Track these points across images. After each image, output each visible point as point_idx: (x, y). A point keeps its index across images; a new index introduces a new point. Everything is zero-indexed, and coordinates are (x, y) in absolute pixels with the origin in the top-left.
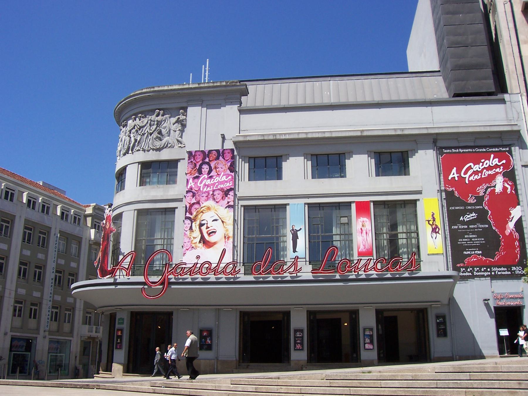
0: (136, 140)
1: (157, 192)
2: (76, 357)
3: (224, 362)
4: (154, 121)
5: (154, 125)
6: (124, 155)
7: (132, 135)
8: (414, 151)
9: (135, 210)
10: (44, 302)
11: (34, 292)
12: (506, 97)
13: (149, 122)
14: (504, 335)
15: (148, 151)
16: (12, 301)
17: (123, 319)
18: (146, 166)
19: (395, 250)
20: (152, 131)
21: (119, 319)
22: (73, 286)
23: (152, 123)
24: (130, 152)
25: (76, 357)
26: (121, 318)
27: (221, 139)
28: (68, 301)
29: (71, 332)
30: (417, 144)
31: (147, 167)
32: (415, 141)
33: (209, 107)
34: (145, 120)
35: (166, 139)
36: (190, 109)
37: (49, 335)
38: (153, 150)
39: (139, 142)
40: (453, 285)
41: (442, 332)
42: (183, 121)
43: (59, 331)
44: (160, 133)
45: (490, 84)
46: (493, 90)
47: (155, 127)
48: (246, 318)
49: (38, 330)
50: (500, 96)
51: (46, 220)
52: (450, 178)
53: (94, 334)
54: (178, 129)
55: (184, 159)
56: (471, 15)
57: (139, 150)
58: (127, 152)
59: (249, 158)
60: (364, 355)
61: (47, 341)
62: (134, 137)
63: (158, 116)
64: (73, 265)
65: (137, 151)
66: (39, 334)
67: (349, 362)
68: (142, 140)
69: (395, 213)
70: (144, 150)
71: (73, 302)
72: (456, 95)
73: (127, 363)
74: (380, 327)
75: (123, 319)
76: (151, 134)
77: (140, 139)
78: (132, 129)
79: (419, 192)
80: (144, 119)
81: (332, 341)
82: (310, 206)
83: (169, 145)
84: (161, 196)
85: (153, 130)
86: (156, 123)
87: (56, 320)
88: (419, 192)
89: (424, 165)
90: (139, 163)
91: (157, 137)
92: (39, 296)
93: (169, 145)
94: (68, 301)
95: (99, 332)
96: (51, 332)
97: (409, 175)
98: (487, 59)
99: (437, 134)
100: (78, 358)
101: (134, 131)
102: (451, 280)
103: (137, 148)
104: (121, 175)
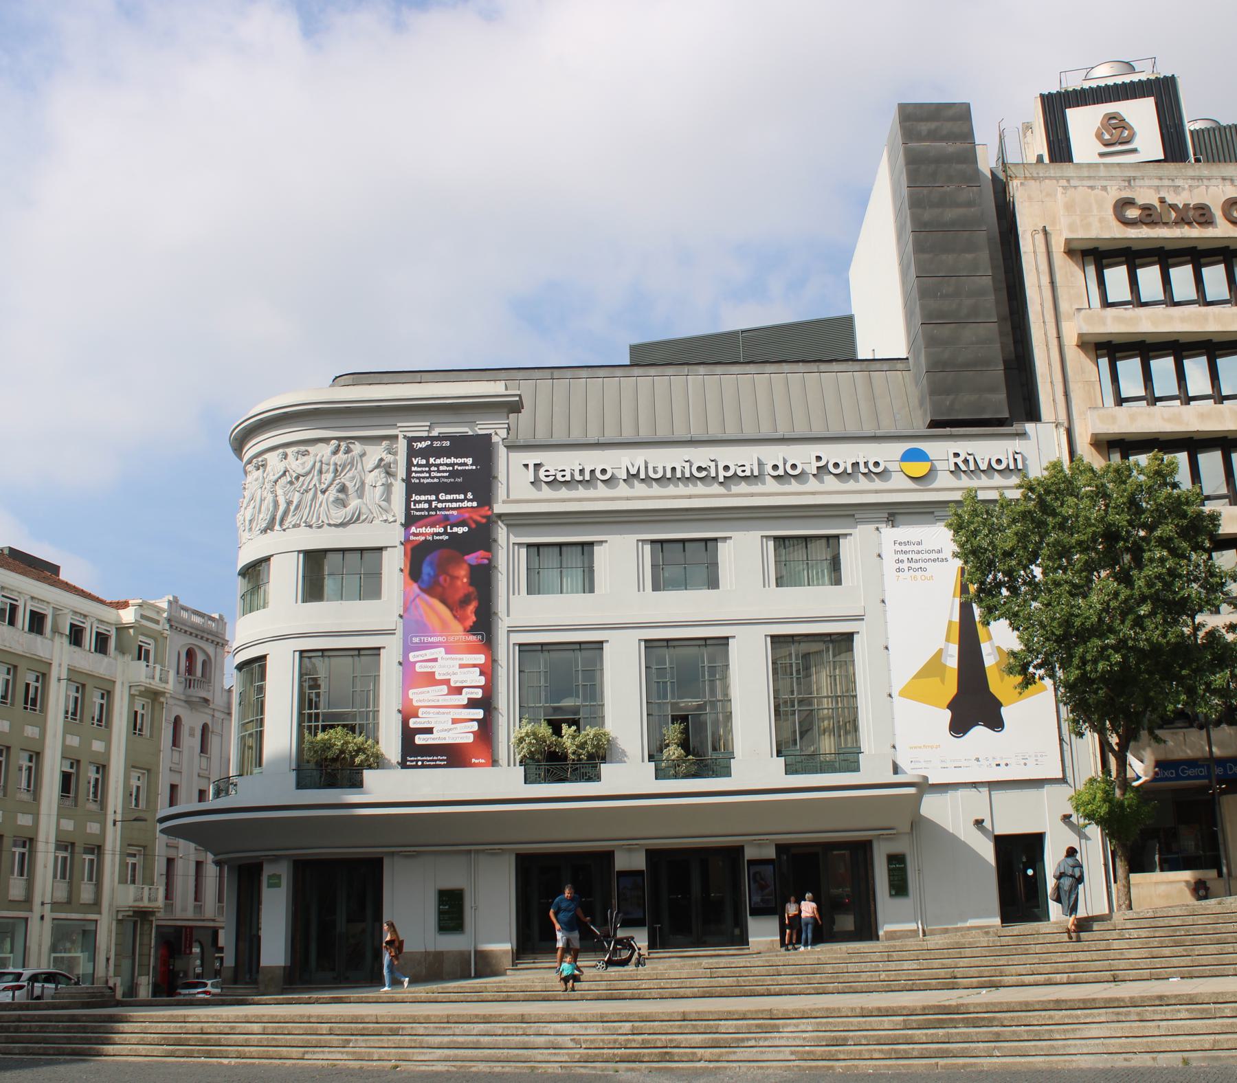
0: (289, 503)
1: (340, 617)
2: (108, 960)
4: (328, 464)
5: (328, 471)
6: (265, 531)
7: (280, 492)
10: (41, 837)
11: (20, 815)
12: (1030, 427)
13: (318, 465)
14: (1158, 876)
16: (52, 847)
17: (279, 877)
18: (314, 561)
20: (324, 486)
21: (270, 877)
23: (325, 468)
24: (277, 527)
25: (108, 960)
26: (274, 875)
28: (88, 831)
29: (96, 905)
31: (314, 561)
34: (309, 461)
35: (354, 503)
37: (52, 911)
38: (329, 525)
39: (297, 507)
40: (918, 800)
41: (899, 887)
42: (389, 465)
43: (70, 902)
44: (343, 489)
45: (998, 402)
46: (1006, 415)
47: (330, 476)
49: (28, 901)
50: (1016, 427)
51: (40, 646)
54: (379, 483)
56: (969, 256)
57: (299, 525)
58: (270, 527)
60: (69, 737)
61: (48, 924)
63: (335, 452)
65: (294, 526)
66: (31, 910)
68: (303, 504)
71: (98, 832)
72: (934, 424)
76: (323, 492)
77: (300, 502)
79: (859, 618)
80: (305, 458)
82: (649, 644)
85: (327, 483)
86: (332, 468)
87: (63, 877)
88: (859, 618)
91: (337, 500)
92: (98, 832)
93: (363, 517)
94: (88, 831)
95: (156, 900)
96: (56, 906)
100: (112, 962)
101: (283, 480)
102: (912, 790)
103: (290, 520)
104: (255, 572)
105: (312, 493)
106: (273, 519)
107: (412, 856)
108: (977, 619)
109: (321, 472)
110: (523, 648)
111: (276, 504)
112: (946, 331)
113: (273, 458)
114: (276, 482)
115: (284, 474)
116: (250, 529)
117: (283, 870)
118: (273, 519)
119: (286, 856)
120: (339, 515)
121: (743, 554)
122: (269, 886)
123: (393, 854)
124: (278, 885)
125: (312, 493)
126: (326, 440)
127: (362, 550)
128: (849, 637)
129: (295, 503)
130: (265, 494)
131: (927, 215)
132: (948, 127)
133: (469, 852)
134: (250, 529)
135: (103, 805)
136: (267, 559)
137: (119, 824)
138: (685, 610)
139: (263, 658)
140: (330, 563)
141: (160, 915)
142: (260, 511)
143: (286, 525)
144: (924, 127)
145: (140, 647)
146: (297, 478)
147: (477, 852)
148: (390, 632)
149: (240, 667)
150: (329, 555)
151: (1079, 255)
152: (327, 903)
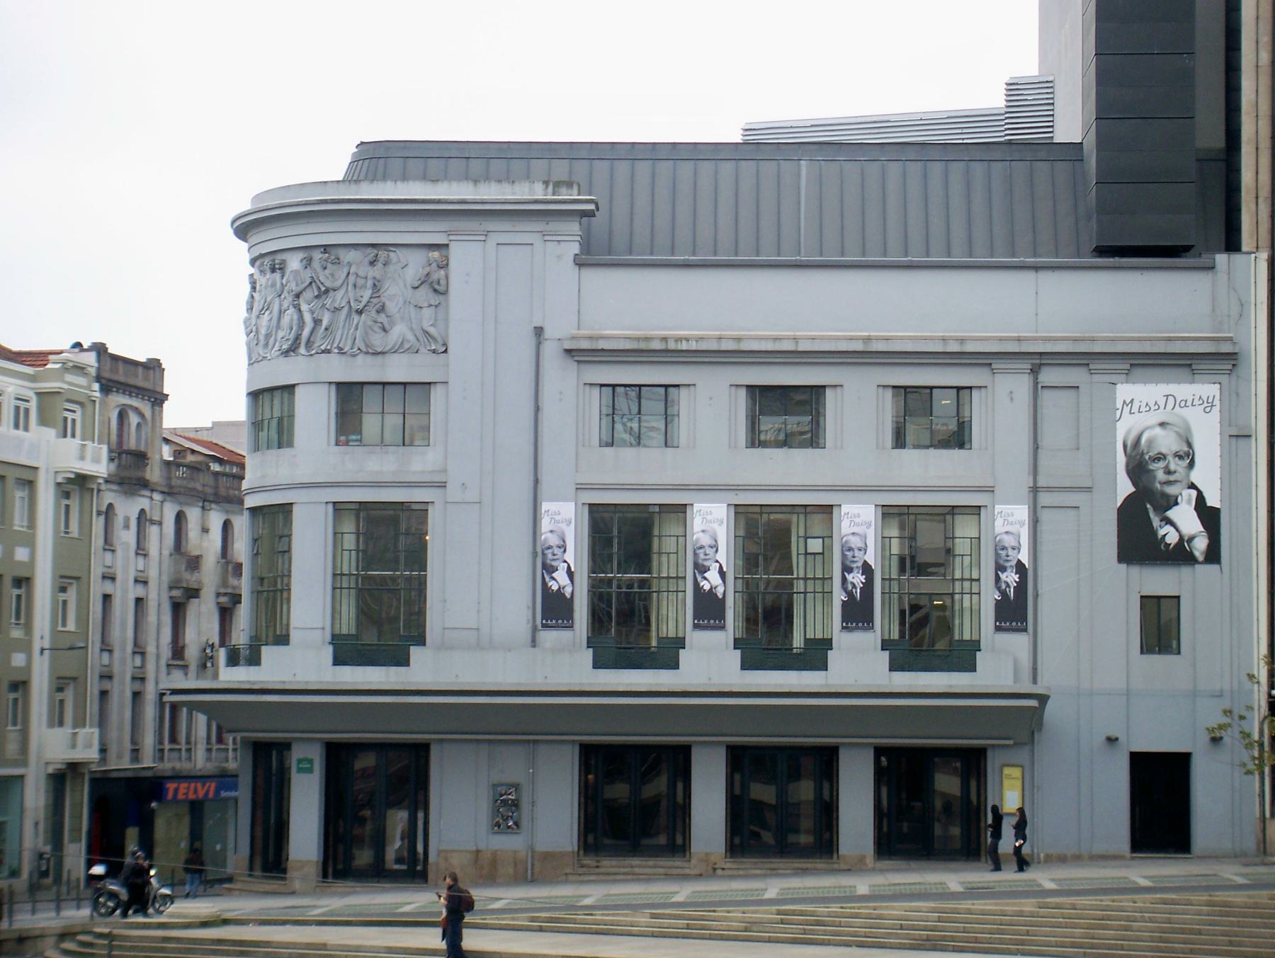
0: (317, 322)
3: (547, 856)
6: (286, 353)
7: (304, 307)
12: (1221, 259)
17: (311, 761)
20: (361, 307)
24: (302, 350)
27: (531, 340)
31: (349, 397)
48: (679, 841)
50: (1204, 260)
53: (79, 755)
57: (329, 352)
58: (292, 350)
59: (602, 385)
60: (1244, 248)
62: (313, 313)
64: (21, 554)
65: (323, 352)
67: (1098, 84)
70: (341, 352)
73: (321, 859)
74: (884, 791)
75: (311, 761)
76: (360, 312)
81: (781, 797)
83: (407, 346)
86: (370, 283)
88: (990, 490)
106: (298, 337)
110: (595, 508)
113: (294, 263)
114: (298, 296)
116: (266, 345)
117: (316, 755)
118: (298, 337)
121: (858, 409)
122: (300, 770)
123: (442, 741)
124: (310, 771)
127: (405, 384)
129: (325, 323)
134: (266, 345)
135: (28, 627)
137: (46, 652)
138: (784, 474)
140: (370, 400)
141: (94, 768)
142: (278, 327)
145: (66, 419)
146: (327, 291)
150: (366, 388)
152: (374, 794)
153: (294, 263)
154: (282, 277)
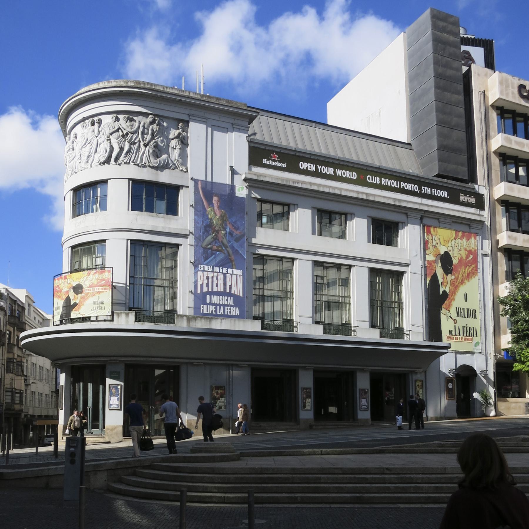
0: (122, 149)
6: (104, 163)
8: (405, 224)
9: (127, 240)
13: (141, 129)
15: (144, 166)
19: (384, 308)
22: (22, 335)
30: (408, 217)
32: (438, 219)
33: (216, 127)
36: (192, 125)
38: (149, 166)
46: (467, 178)
47: (149, 137)
52: (441, 293)
55: (188, 187)
57: (129, 163)
58: (107, 161)
65: (125, 163)
69: (385, 279)
76: (145, 146)
78: (115, 132)
84: (163, 228)
85: (147, 140)
86: (150, 132)
88: (407, 265)
89: (409, 236)
90: (130, 179)
97: (396, 246)
98: (463, 146)
99: (425, 211)
105: (137, 144)
106: (109, 157)
107: (195, 365)
108: (12, 428)
109: (143, 133)
111: (112, 148)
112: (446, 130)
113: (107, 120)
115: (118, 130)
118: (109, 157)
119: (123, 361)
120: (154, 162)
125: (137, 144)
126: (146, 115)
128: (402, 274)
130: (100, 141)
131: (440, 70)
132: (450, 27)
133: (229, 365)
136: (104, 182)
139: (104, 241)
143: (120, 161)
144: (441, 24)
147: (232, 365)
148: (185, 236)
149: (73, 247)
151: (495, 108)
153: (107, 120)
154: (99, 127)
